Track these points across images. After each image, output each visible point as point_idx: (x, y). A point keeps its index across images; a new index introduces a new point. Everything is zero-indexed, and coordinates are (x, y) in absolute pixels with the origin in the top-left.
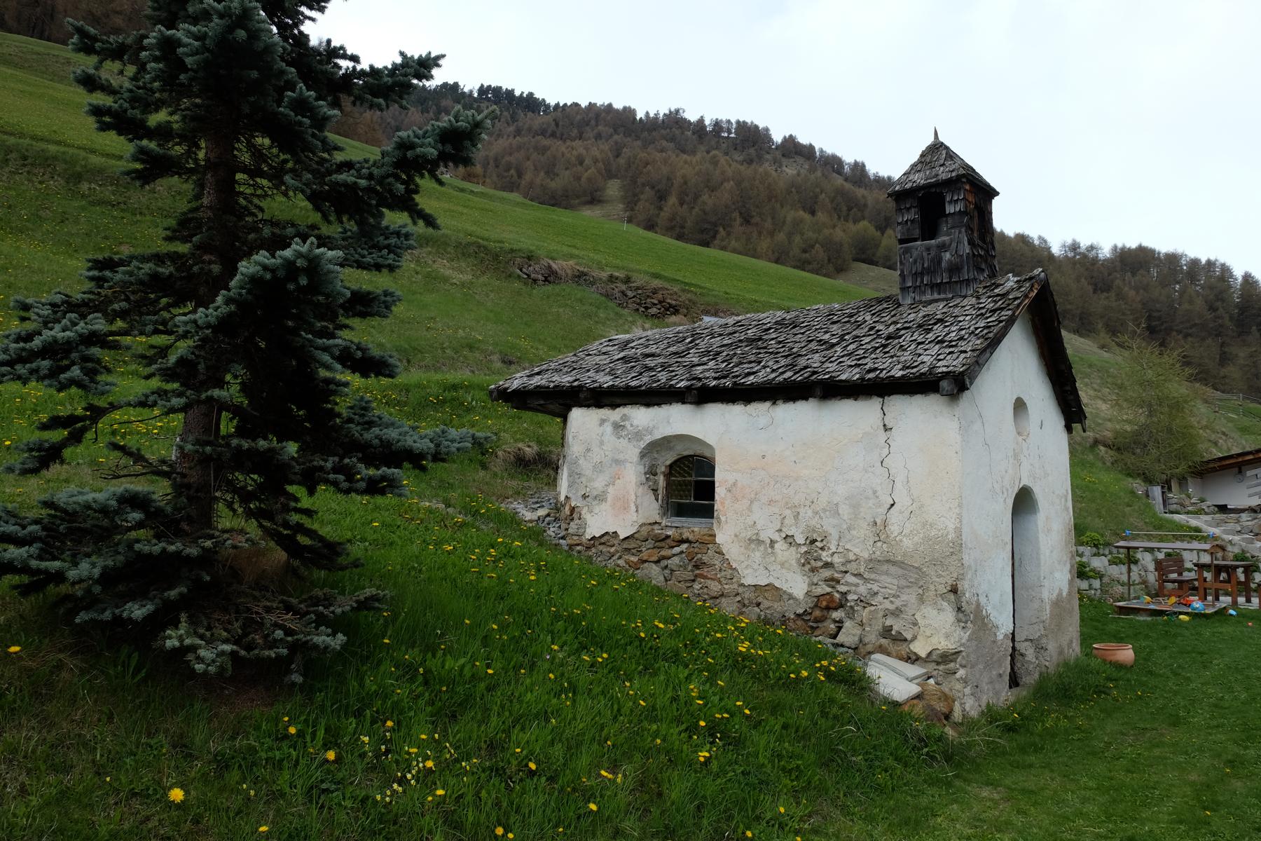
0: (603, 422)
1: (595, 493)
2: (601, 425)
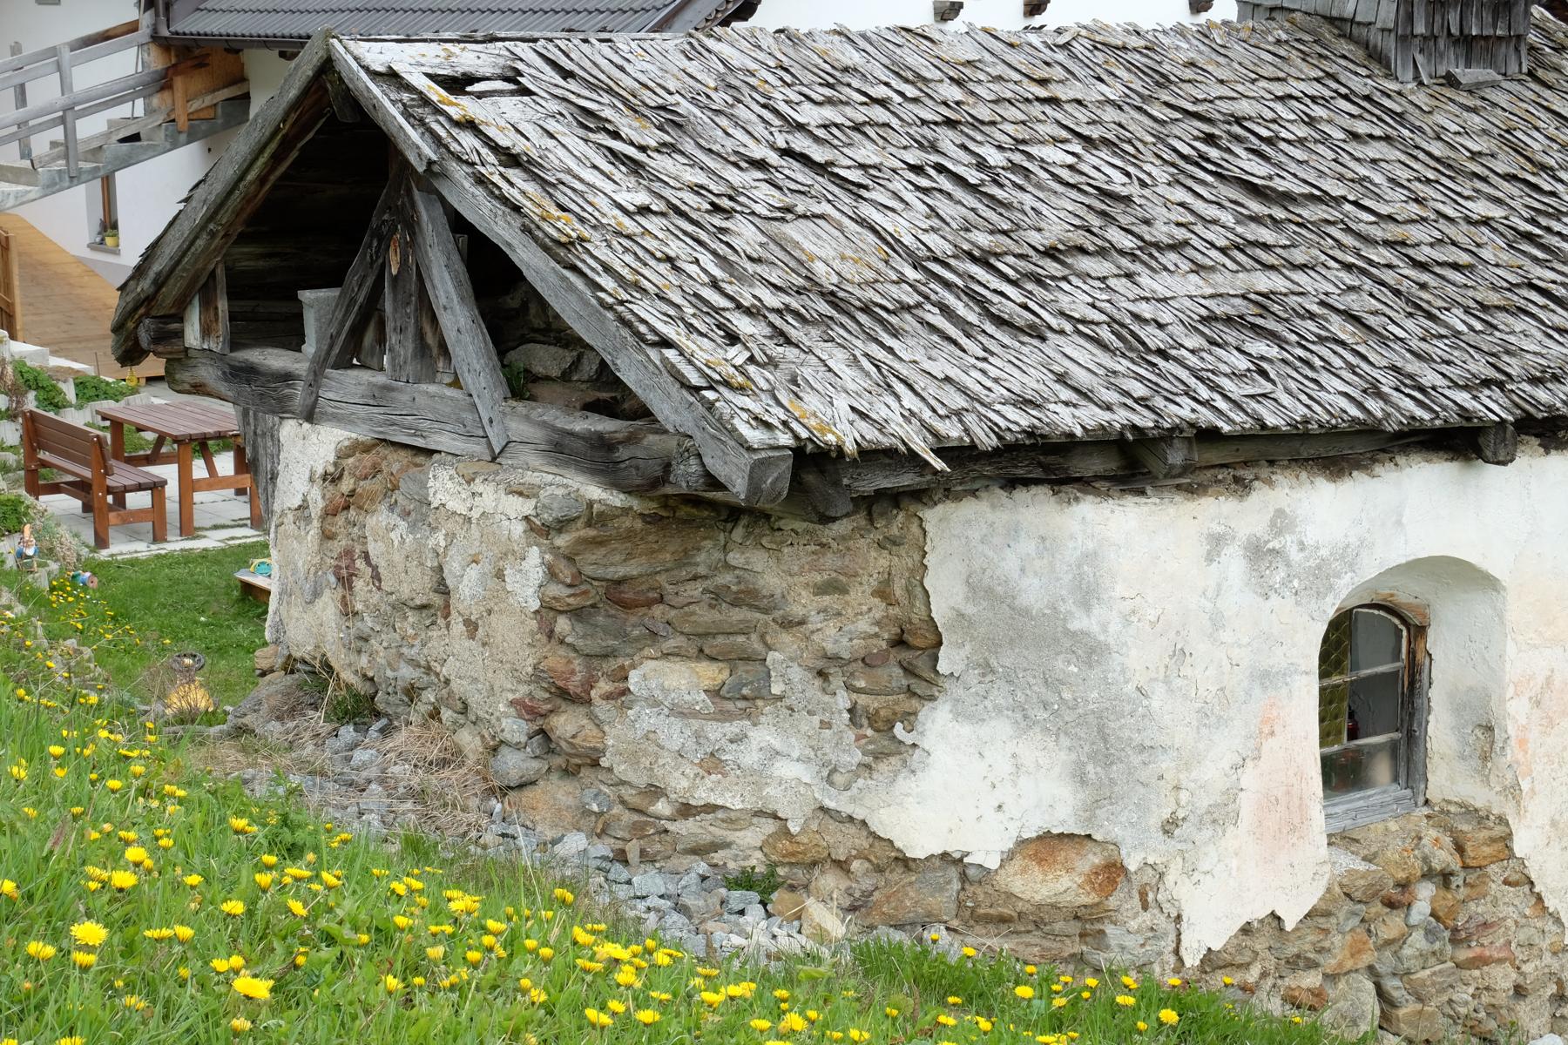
0: (1217, 542)
1: (1204, 803)
2: (1210, 559)
